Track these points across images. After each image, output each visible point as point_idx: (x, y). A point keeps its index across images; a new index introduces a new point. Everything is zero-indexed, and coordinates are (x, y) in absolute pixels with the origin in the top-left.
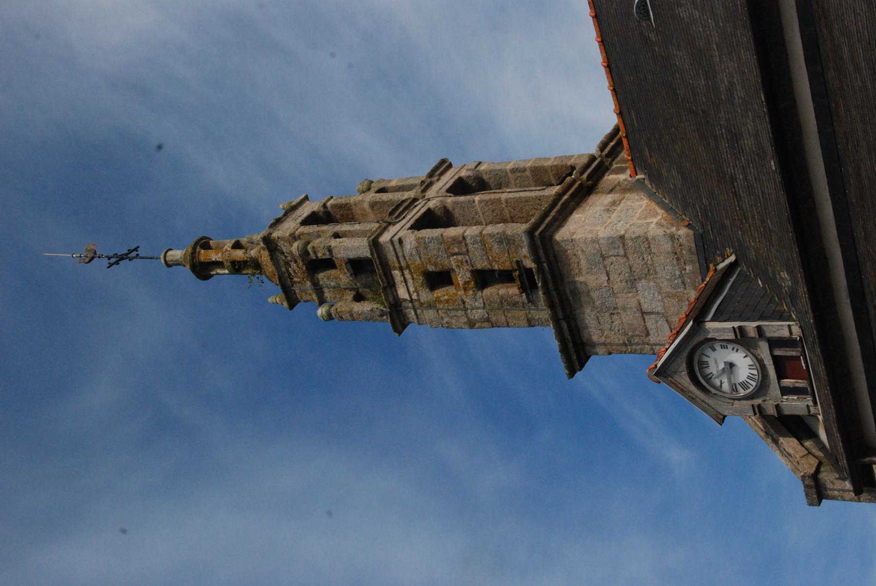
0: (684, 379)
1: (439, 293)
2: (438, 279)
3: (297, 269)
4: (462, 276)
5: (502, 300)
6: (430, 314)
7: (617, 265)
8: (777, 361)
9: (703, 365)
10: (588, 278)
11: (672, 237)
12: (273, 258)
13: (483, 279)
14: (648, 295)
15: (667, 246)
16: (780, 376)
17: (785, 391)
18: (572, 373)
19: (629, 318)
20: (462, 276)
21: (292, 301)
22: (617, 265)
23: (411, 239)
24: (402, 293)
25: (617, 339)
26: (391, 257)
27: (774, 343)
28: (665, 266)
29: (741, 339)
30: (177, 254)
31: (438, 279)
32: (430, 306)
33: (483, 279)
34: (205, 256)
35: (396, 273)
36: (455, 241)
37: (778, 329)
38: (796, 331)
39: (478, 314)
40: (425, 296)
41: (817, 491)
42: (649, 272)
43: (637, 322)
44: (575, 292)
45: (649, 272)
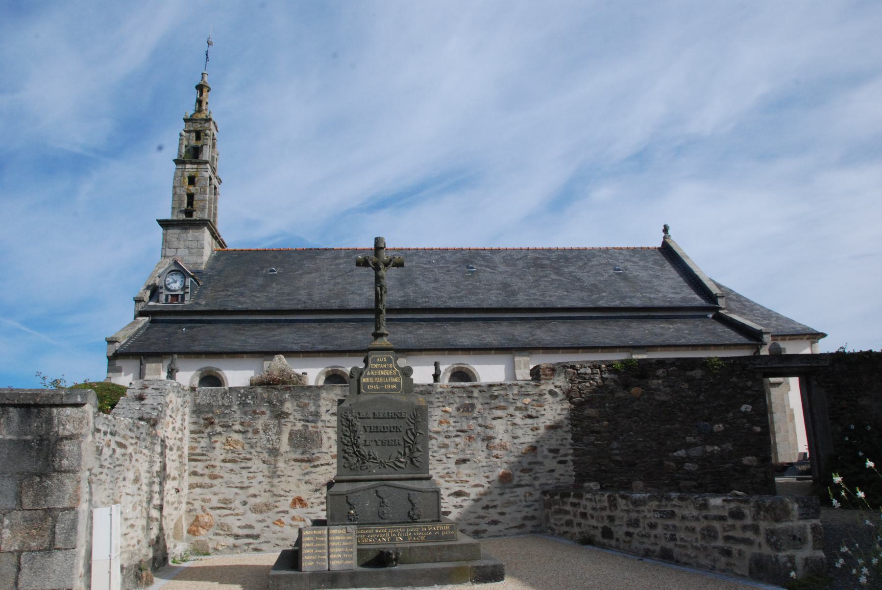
0: (173, 268)
1: (187, 179)
2: (192, 181)
3: (198, 126)
4: (192, 189)
5: (183, 201)
6: (179, 174)
7: (194, 244)
8: (177, 296)
9: (176, 274)
10: (191, 234)
11: (202, 264)
12: (203, 119)
13: (191, 197)
14: (182, 252)
15: (199, 261)
16: (172, 295)
17: (167, 296)
18: (159, 221)
19: (175, 243)
20: (192, 189)
21: (186, 120)
22: (194, 244)
23: (207, 175)
24: (188, 166)
25: (168, 238)
26: (202, 166)
27: (183, 296)
28: (193, 259)
29: (184, 287)
30: (206, 78)
31: (192, 181)
32: (183, 175)
33: (191, 197)
34: (205, 90)
35: (195, 166)
36: (205, 191)
37: (187, 297)
38: (186, 303)
39: (178, 190)
40: (186, 174)
41: (138, 301)
42: (191, 254)
43: (174, 246)
44: (186, 229)
45: (191, 254)
